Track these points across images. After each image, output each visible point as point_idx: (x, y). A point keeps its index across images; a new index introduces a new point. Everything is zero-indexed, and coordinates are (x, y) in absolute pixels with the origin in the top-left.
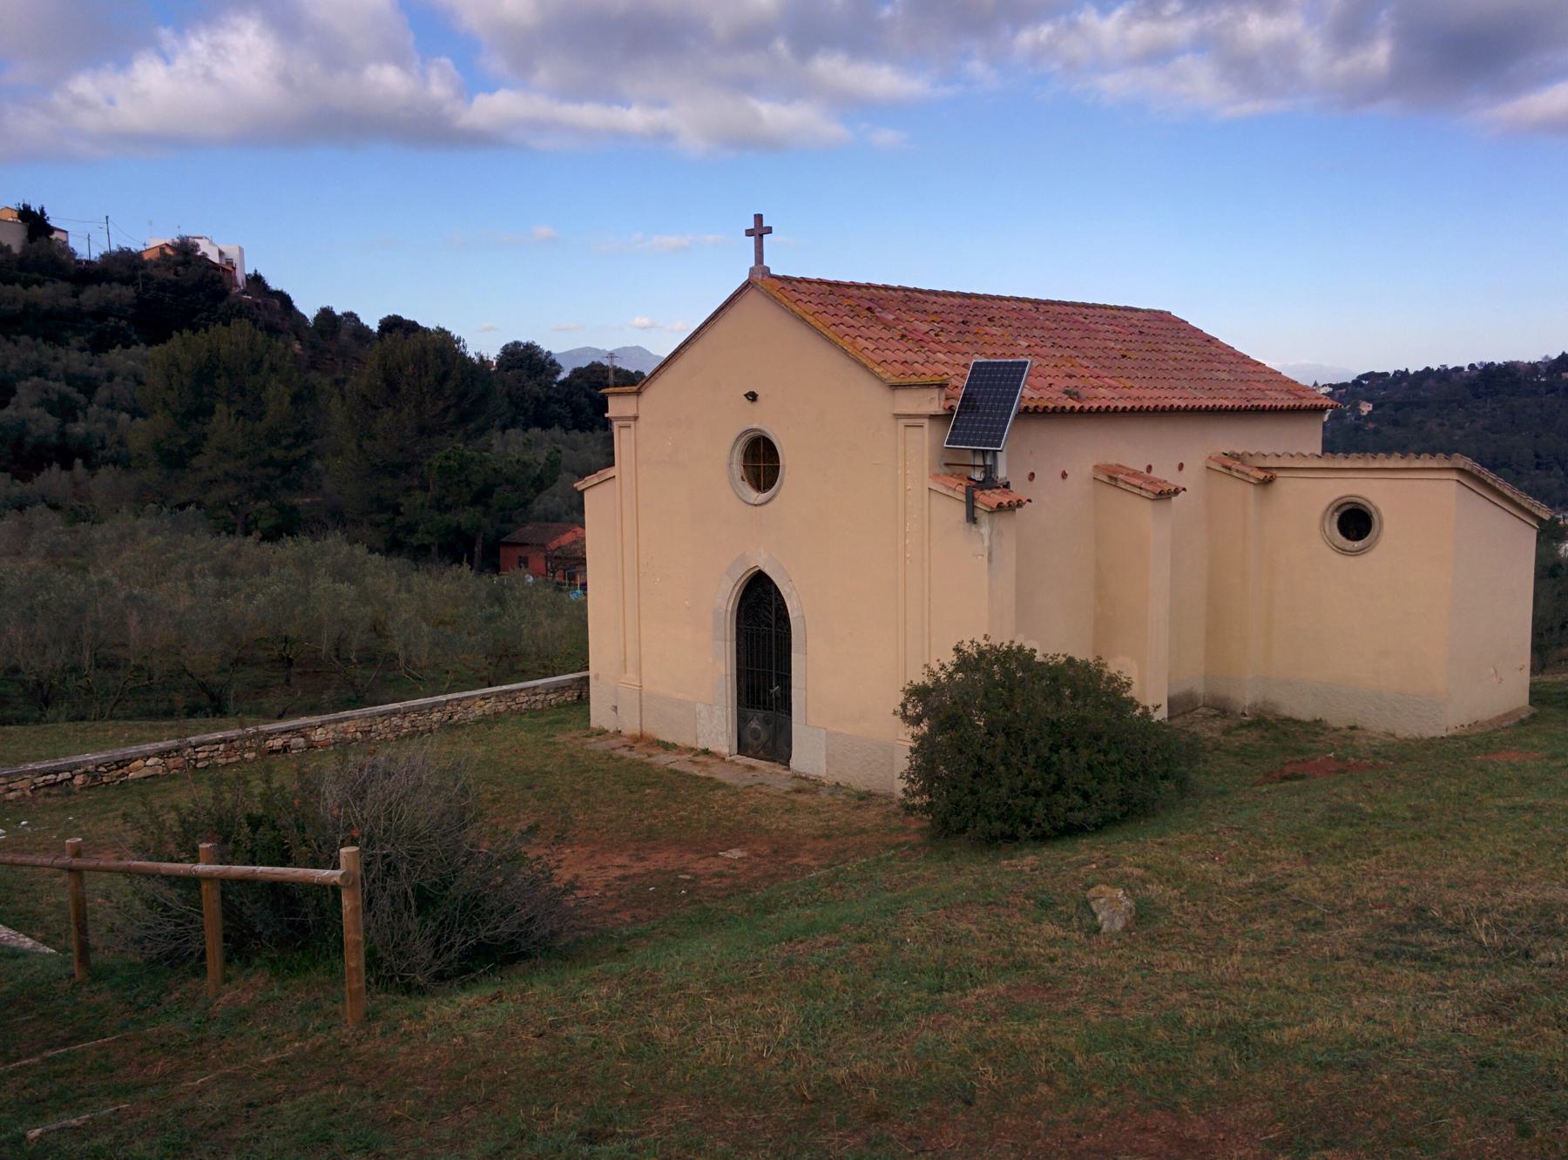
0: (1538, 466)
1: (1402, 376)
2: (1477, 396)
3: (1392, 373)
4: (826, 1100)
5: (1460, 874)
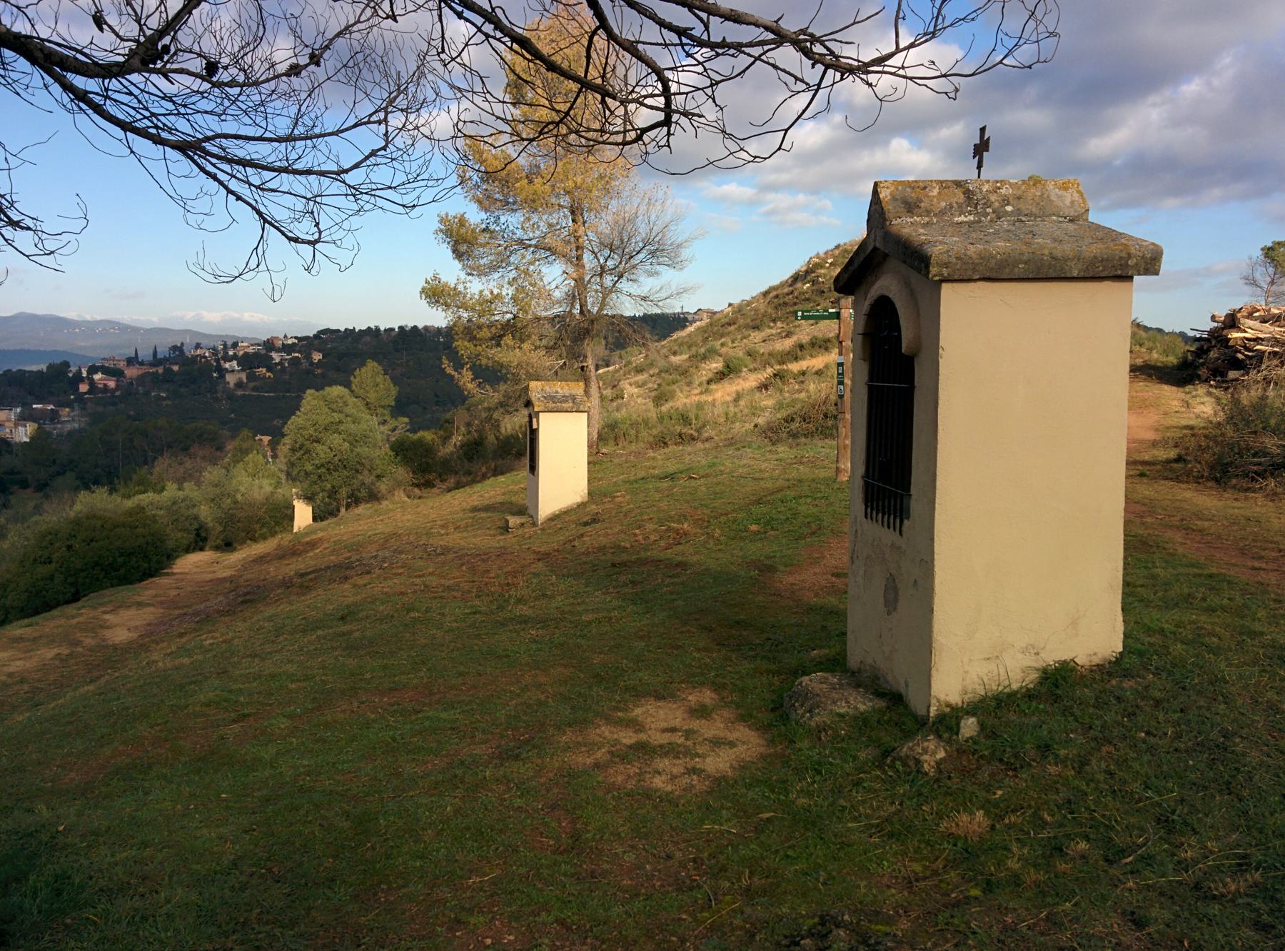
0: (437, 403)
1: (349, 333)
2: (397, 351)
3: (342, 329)
4: (632, 847)
5: (232, 596)
